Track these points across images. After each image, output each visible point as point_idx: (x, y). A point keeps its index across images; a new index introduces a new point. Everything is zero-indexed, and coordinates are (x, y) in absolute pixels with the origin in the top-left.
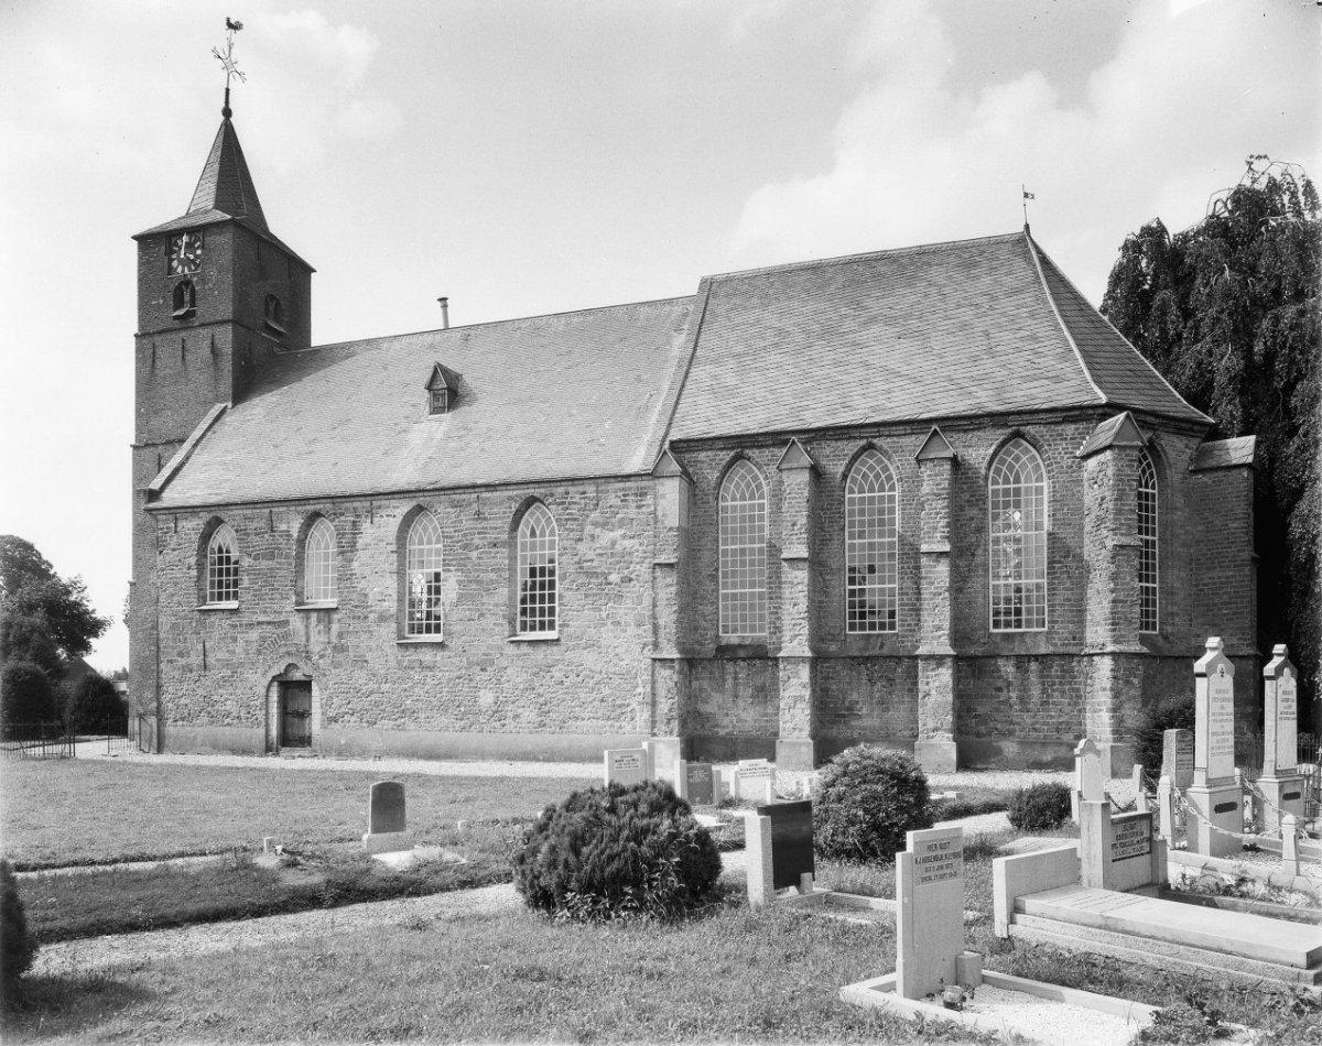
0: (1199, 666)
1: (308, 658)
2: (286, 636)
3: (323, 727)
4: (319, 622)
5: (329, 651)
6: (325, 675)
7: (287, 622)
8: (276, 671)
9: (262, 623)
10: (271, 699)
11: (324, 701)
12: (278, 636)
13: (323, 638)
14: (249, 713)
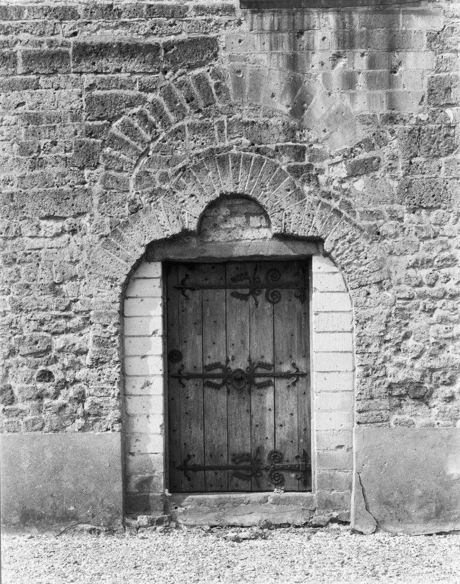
0: (167, 490)
1: (304, 172)
2: (204, 97)
3: (368, 417)
4: (346, 41)
5: (395, 145)
6: (377, 235)
7: (203, 48)
8: (161, 223)
9: (101, 50)
10: (133, 327)
11: (373, 329)
12: (169, 95)
13: (364, 102)
14: (46, 376)
